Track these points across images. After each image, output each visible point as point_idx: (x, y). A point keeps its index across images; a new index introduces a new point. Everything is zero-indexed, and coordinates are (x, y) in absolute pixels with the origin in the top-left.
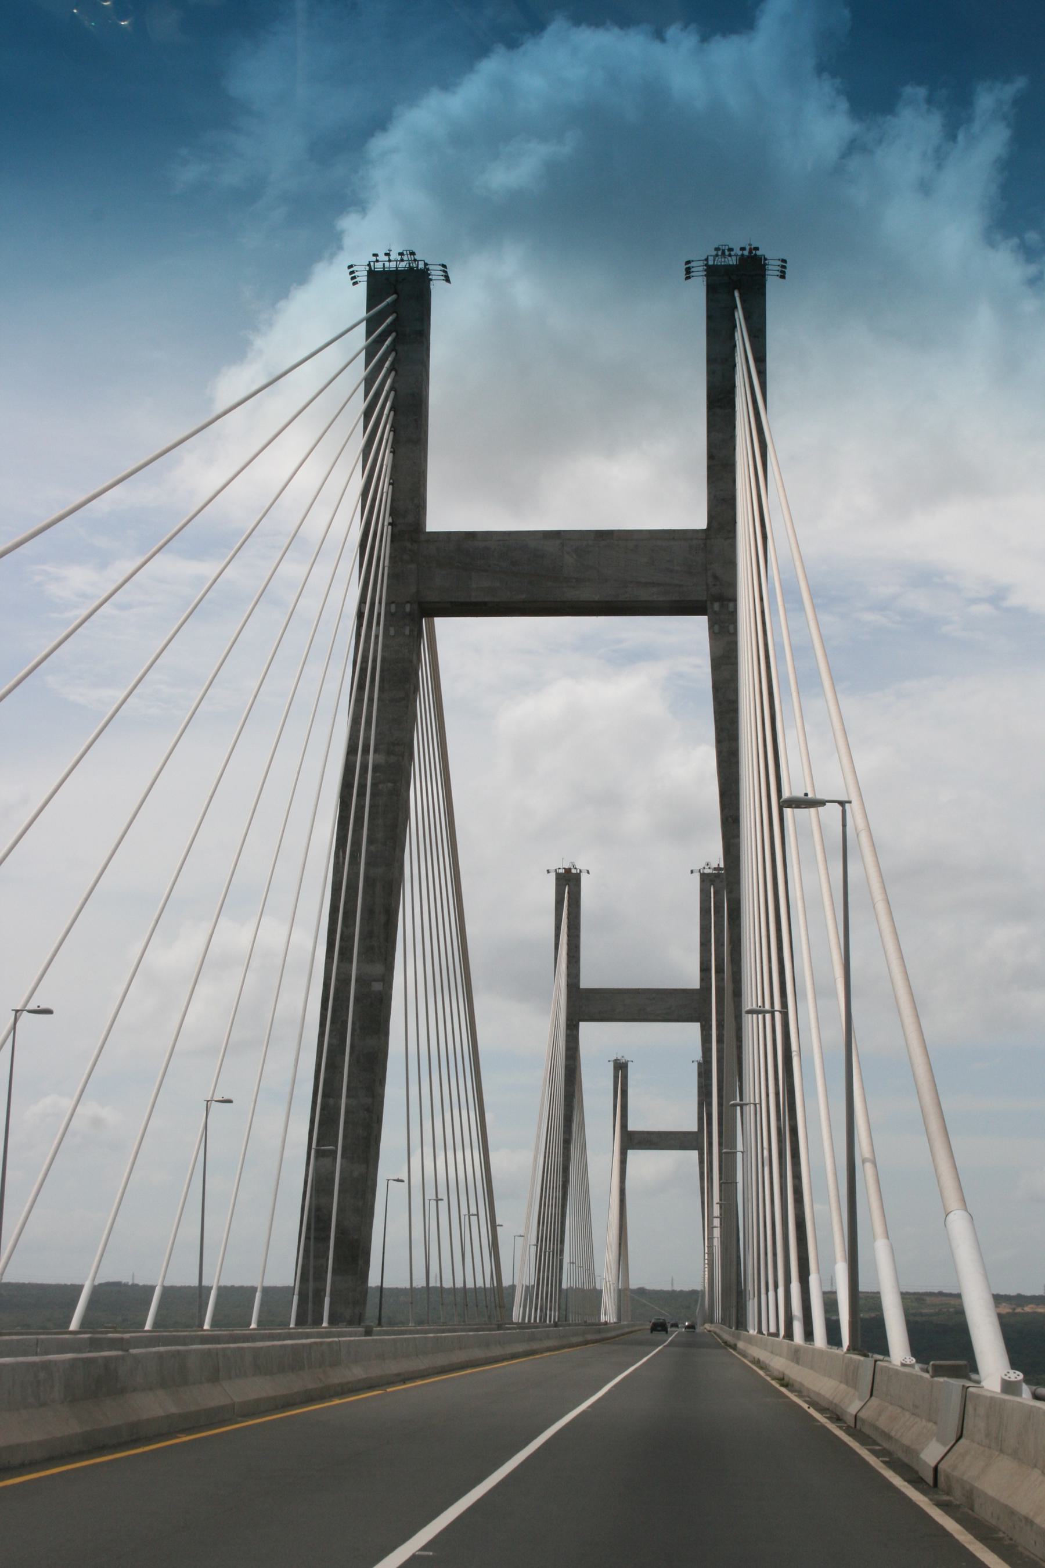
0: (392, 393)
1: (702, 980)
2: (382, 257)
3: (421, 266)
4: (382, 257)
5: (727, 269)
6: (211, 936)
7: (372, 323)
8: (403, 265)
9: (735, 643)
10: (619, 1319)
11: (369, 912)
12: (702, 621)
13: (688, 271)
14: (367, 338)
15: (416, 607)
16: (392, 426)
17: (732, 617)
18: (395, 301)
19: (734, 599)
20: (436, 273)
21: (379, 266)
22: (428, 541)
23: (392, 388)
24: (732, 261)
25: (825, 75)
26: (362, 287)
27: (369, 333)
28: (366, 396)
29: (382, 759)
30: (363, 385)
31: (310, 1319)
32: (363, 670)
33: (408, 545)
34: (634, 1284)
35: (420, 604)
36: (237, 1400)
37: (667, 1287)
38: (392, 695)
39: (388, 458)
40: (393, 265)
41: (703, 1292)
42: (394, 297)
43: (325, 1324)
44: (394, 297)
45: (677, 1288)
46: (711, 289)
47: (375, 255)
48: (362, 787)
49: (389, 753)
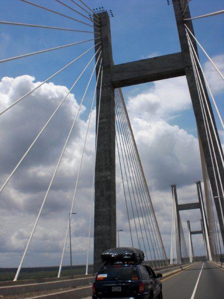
20: (110, 14)
34: (195, 256)
43: (87, 274)
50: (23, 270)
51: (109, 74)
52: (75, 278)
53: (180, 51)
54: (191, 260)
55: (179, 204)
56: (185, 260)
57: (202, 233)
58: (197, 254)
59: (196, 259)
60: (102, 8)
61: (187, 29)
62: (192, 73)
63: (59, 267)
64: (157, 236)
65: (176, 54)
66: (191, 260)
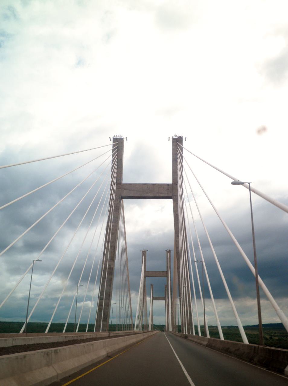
0: (117, 159)
1: (167, 269)
2: (115, 136)
3: (122, 137)
4: (115, 136)
5: (176, 139)
6: (58, 157)
7: (113, 150)
8: (119, 137)
9: (178, 204)
10: (151, 330)
11: (111, 252)
12: (172, 200)
13: (169, 139)
14: (113, 152)
15: (120, 197)
16: (117, 165)
17: (177, 199)
18: (118, 143)
19: (177, 196)
20: (125, 139)
21: (115, 137)
22: (123, 185)
23: (117, 158)
24: (177, 137)
25: (179, 138)
26: (112, 141)
27: (112, 157)
28: (112, 163)
29: (114, 224)
30: (111, 156)
31: (125, 329)
32: (111, 208)
33: (119, 186)
34: (154, 323)
35: (121, 196)
36: (59, 372)
37: (159, 324)
38: (116, 213)
39: (116, 170)
40: (117, 137)
41: (166, 325)
42: (117, 143)
43: (101, 331)
44: (117, 143)
45: (160, 324)
46: (173, 142)
47: (114, 135)
48: (112, 215)
49: (115, 223)
50: (52, 325)
51: (120, 189)
52: (29, 336)
53: (172, 183)
54: (150, 329)
55: (126, 180)
56: (145, 327)
57: (165, 300)
58: (156, 323)
59: (155, 327)
60: (121, 135)
61: (179, 149)
62: (177, 197)
63: (48, 324)
64: (129, 305)
65: (168, 185)
66: (150, 329)
